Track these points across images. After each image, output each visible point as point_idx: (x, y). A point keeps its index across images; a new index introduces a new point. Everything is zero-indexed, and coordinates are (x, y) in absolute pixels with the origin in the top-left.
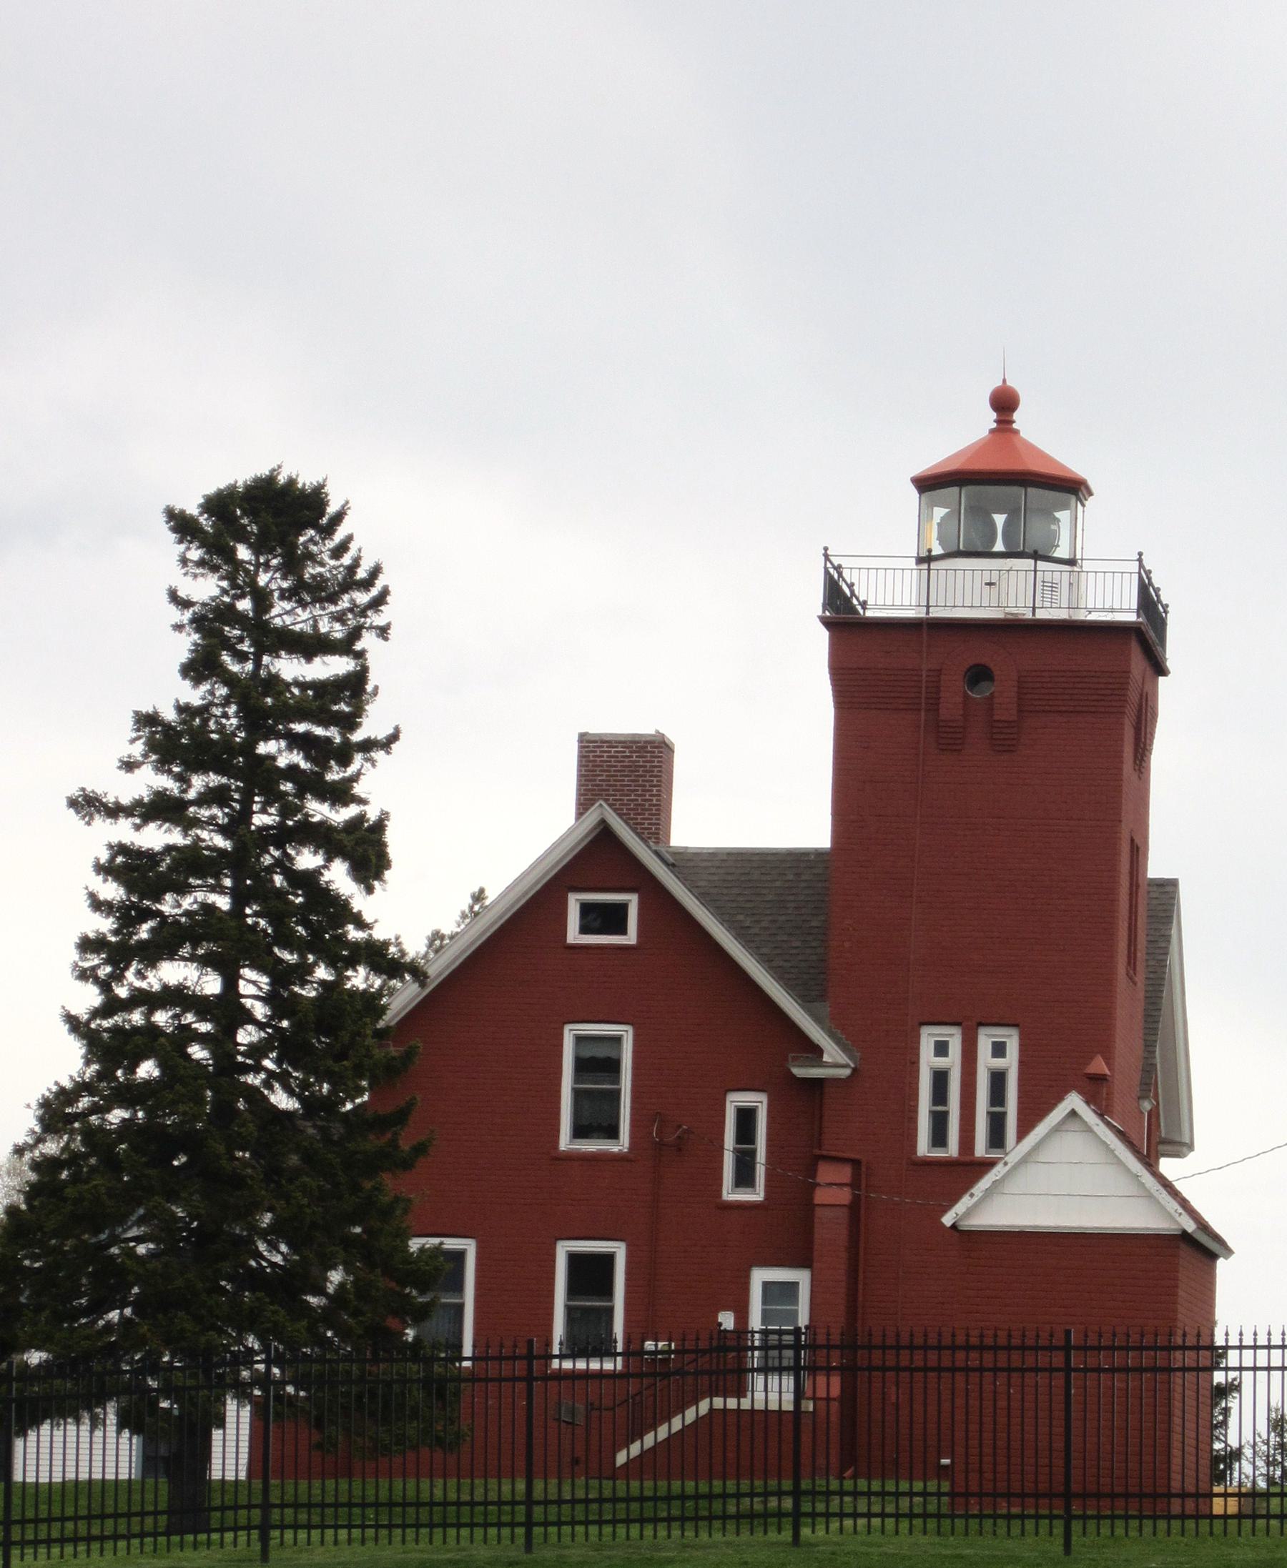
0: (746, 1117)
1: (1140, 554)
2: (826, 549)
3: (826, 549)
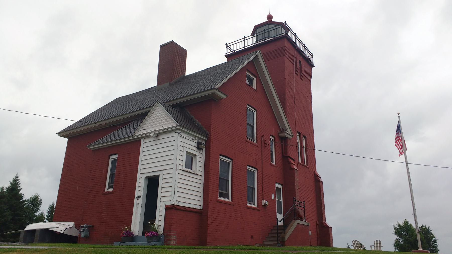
2: (226, 43)
3: (226, 43)
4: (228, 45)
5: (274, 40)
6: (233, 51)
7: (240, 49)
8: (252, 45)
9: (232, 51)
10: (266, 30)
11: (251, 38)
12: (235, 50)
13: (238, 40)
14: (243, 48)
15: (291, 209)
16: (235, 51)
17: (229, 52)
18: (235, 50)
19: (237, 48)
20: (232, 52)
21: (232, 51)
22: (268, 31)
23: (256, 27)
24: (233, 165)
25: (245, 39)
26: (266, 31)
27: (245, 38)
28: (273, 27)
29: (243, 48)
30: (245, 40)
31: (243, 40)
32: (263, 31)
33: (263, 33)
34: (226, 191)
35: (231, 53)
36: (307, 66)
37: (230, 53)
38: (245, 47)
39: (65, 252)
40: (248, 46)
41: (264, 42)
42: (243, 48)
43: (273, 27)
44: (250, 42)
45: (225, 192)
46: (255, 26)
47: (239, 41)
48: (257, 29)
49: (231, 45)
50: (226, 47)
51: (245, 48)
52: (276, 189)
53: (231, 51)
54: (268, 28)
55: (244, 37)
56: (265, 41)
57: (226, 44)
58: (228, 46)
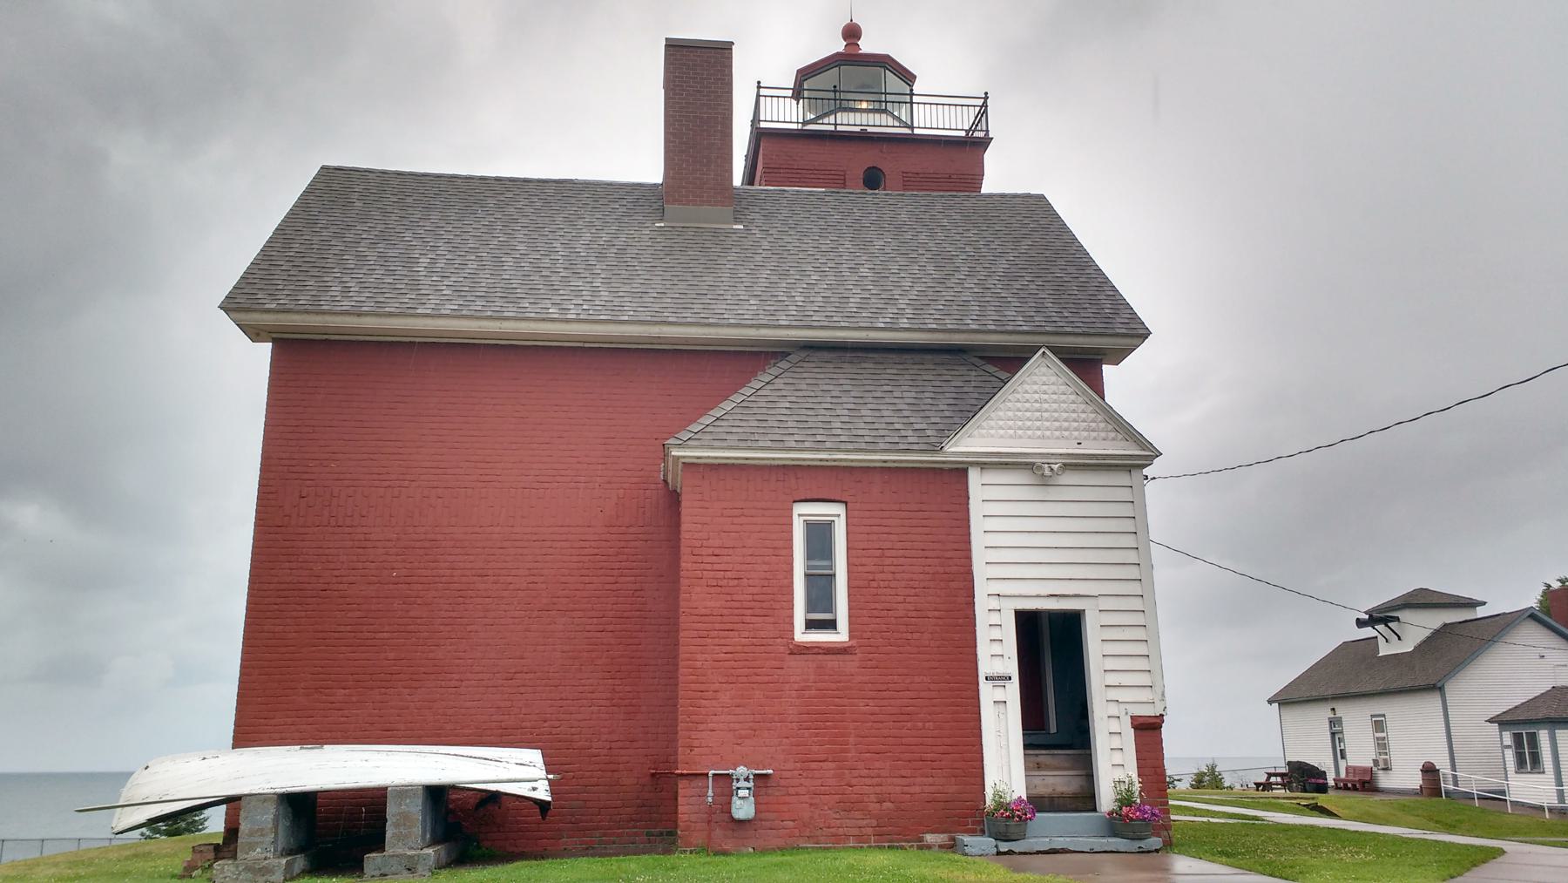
0: (819, 535)
1: (986, 93)
2: (759, 83)
3: (759, 83)
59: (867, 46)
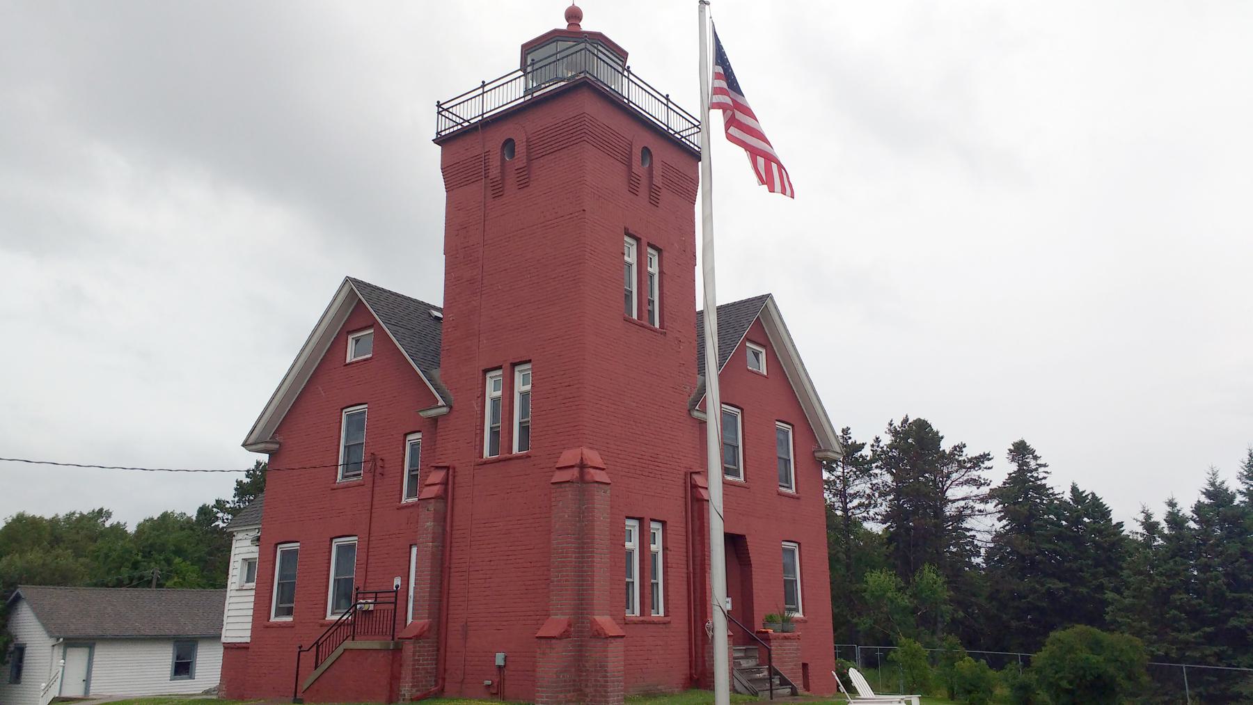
2: (438, 102)
3: (438, 102)
4: (444, 106)
5: (551, 95)
6: (465, 121)
7: (511, 102)
8: (522, 100)
9: (462, 121)
10: (538, 62)
11: (520, 77)
12: (471, 119)
13: (460, 96)
14: (480, 118)
15: (655, 576)
16: (472, 121)
17: (447, 126)
18: (471, 119)
19: (470, 112)
20: (460, 127)
21: (462, 121)
22: (555, 59)
23: (527, 49)
24: (480, 433)
25: (486, 88)
26: (487, 86)
27: (484, 85)
28: (567, 49)
29: (479, 116)
30: (484, 93)
31: (480, 91)
32: (479, 88)
33: (581, 48)
34: (220, 546)
35: (456, 128)
36: (678, 160)
37: (451, 130)
38: (483, 114)
39: (159, 617)
40: (511, 102)
41: (483, 119)
42: (479, 116)
43: (567, 49)
44: (514, 93)
45: (734, 467)
46: (523, 46)
47: (475, 92)
48: (529, 53)
49: (452, 107)
50: (439, 113)
51: (485, 116)
52: (14, 595)
53: (458, 124)
54: (555, 52)
55: (483, 82)
56: (535, 95)
57: (439, 105)
58: (447, 110)
59: (586, 25)
